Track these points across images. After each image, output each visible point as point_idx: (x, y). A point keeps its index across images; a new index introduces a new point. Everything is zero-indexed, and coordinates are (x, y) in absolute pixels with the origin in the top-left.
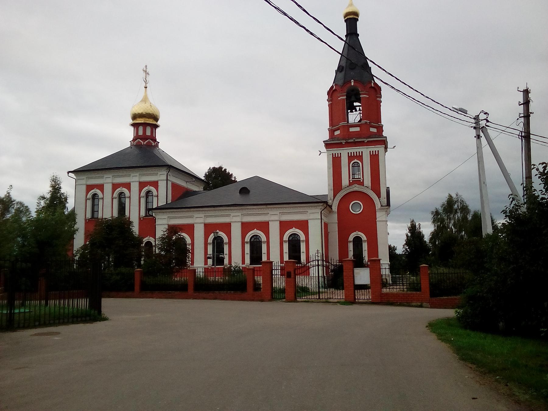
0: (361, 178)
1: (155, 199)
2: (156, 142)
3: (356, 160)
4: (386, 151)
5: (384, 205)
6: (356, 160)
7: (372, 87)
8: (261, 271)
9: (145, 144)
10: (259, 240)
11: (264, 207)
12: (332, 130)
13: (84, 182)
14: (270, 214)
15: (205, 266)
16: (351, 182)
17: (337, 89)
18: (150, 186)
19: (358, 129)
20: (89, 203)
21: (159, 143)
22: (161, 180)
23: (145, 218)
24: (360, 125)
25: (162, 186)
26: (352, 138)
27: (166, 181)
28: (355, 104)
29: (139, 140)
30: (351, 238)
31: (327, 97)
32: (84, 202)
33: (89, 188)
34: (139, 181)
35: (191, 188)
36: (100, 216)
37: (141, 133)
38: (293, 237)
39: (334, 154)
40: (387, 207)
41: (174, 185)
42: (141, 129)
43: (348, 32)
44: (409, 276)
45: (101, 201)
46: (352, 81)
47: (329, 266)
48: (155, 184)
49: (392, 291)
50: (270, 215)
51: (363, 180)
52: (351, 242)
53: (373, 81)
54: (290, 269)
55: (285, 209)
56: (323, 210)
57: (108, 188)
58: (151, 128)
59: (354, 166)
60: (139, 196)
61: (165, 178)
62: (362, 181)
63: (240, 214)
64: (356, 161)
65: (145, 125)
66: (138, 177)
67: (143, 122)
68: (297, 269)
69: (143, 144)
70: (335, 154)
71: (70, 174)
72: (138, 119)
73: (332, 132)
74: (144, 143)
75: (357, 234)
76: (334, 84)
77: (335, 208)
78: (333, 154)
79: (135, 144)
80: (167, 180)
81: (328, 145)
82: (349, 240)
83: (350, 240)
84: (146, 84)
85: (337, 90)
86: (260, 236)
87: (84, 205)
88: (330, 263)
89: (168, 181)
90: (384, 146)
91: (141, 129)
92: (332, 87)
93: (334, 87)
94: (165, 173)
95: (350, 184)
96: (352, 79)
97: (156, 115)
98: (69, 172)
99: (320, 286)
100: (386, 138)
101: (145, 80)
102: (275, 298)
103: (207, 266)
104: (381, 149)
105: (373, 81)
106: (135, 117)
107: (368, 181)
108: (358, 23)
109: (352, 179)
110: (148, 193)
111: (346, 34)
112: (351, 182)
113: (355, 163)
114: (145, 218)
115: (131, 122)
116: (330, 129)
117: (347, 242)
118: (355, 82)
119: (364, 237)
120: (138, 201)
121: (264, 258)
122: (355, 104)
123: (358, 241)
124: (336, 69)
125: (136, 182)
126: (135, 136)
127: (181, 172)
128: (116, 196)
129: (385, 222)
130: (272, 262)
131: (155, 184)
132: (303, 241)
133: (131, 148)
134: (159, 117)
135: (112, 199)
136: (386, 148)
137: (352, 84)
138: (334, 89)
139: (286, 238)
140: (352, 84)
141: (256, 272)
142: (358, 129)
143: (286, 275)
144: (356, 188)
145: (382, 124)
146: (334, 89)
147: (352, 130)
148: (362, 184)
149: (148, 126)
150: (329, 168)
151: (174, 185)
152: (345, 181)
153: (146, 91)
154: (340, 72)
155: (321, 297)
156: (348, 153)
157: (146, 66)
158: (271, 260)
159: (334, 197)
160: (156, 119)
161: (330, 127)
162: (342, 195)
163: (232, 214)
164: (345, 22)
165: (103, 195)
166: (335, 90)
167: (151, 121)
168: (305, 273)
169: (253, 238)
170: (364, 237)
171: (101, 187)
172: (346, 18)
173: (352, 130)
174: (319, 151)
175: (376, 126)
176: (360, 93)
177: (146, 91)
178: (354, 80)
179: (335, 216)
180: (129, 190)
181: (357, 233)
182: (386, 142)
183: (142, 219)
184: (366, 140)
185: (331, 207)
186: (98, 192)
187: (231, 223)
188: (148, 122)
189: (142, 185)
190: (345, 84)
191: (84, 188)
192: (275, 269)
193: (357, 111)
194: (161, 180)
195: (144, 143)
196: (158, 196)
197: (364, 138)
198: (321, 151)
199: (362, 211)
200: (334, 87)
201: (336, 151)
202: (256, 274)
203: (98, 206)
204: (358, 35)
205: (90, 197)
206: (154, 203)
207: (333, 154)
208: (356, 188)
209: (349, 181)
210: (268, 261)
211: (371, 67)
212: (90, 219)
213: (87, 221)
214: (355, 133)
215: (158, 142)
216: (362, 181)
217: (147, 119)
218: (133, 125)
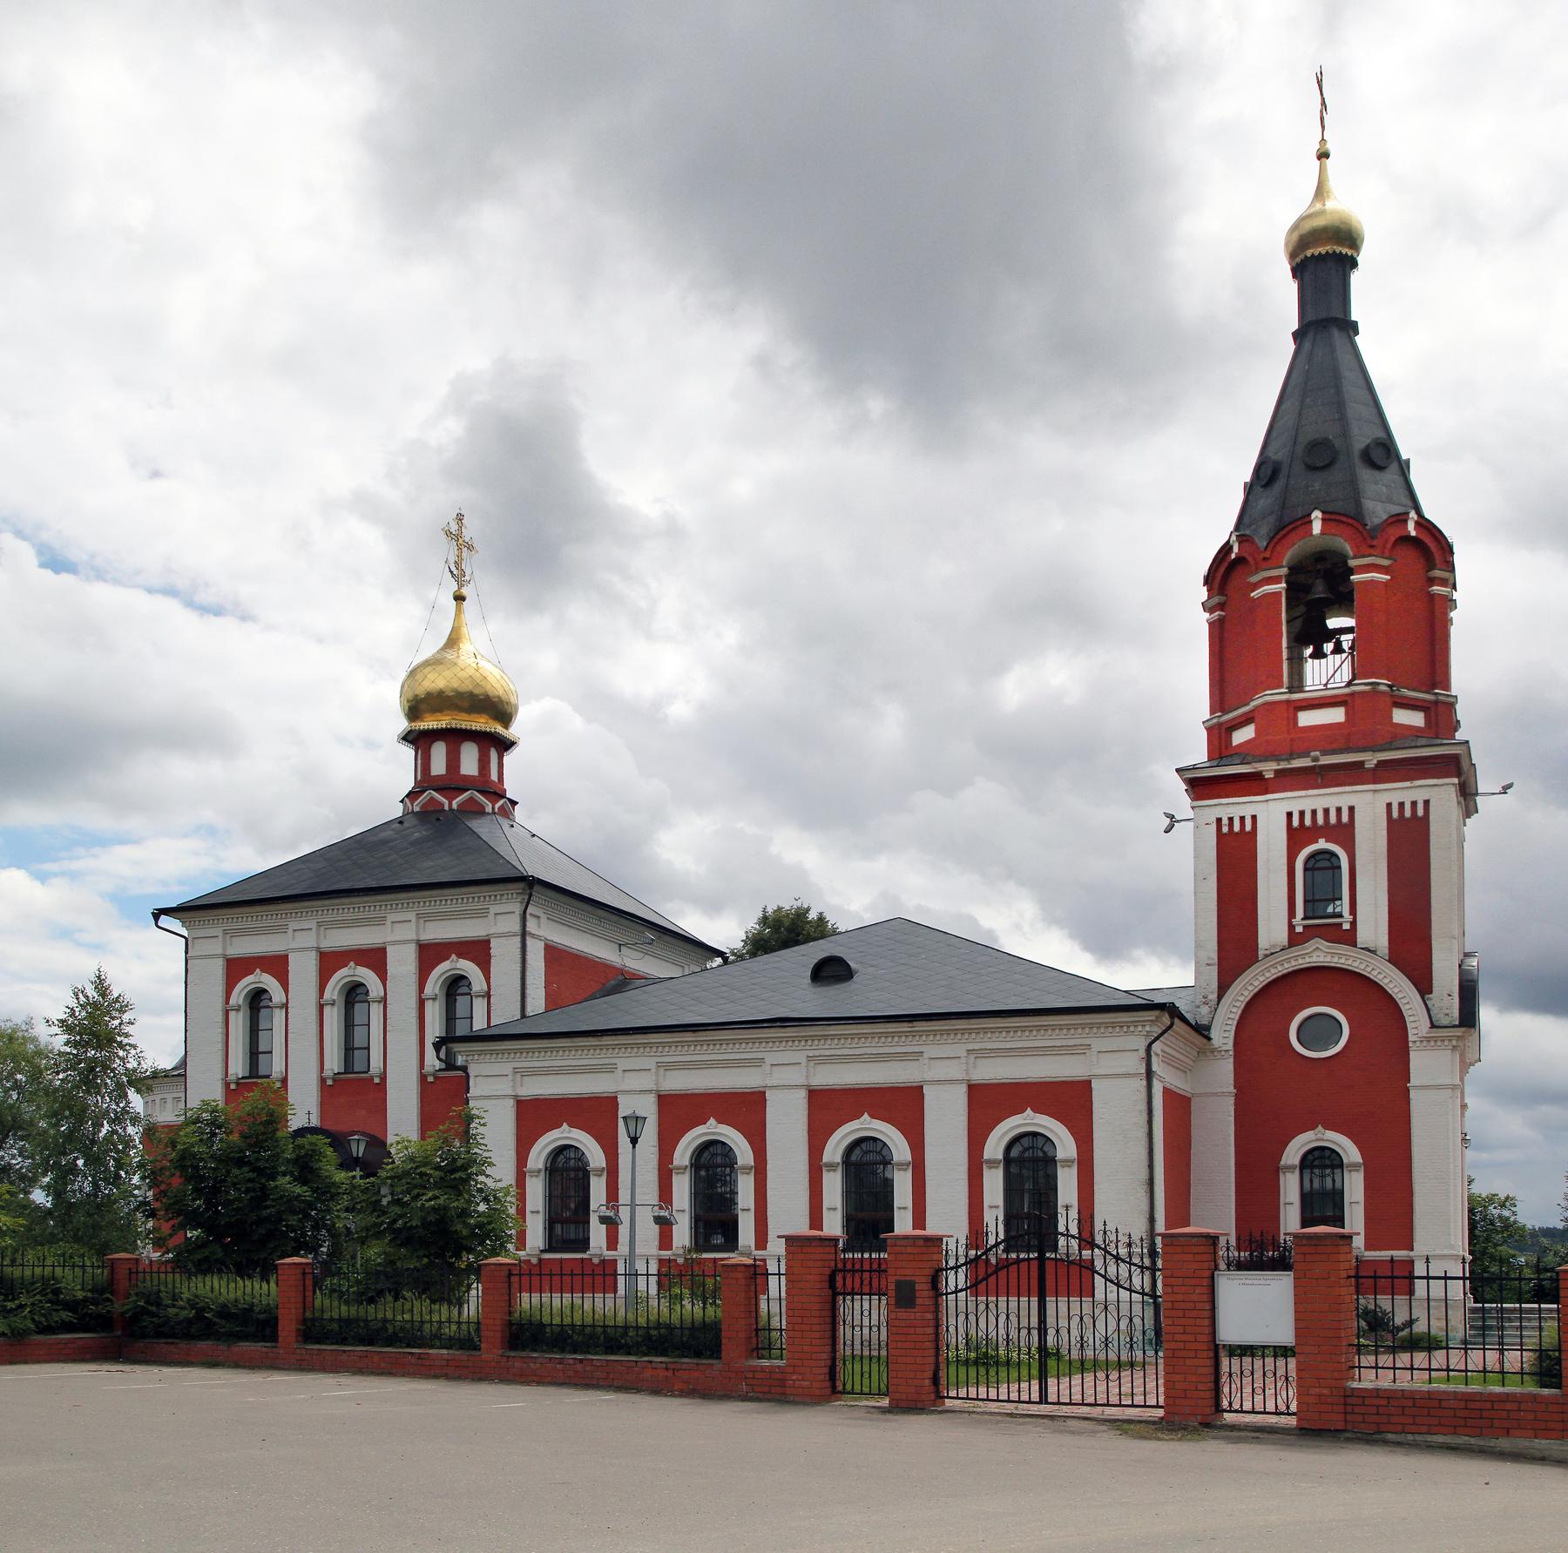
0: (1346, 913)
1: (479, 1006)
2: (501, 802)
4: (1469, 809)
5: (1445, 1022)
7: (1408, 538)
8: (1375, 1272)
9: (455, 806)
10: (883, 1157)
11: (905, 1027)
12: (1220, 725)
13: (216, 947)
14: (925, 1056)
15: (663, 1252)
16: (1299, 929)
17: (1246, 555)
18: (460, 956)
19: (1336, 715)
20: (239, 1022)
21: (514, 803)
22: (500, 936)
23: (441, 1074)
24: (1347, 698)
25: (504, 954)
26: (1305, 754)
27: (518, 939)
28: (1333, 623)
29: (432, 791)
30: (1293, 1152)
31: (1203, 593)
32: (220, 1018)
33: (236, 968)
34: (418, 941)
35: (585, 950)
36: (278, 1070)
37: (439, 766)
38: (1026, 1145)
39: (1225, 821)
40: (1459, 1032)
41: (554, 955)
42: (439, 752)
43: (1310, 317)
45: (279, 1015)
46: (1412, 518)
47: (1093, 1261)
48: (479, 951)
49: (1404, 1382)
50: (926, 1061)
51: (1354, 923)
52: (1290, 1168)
53: (1413, 515)
54: (908, 1272)
55: (989, 1035)
56: (1157, 1039)
57: (303, 969)
58: (480, 751)
59: (1313, 869)
60: (420, 996)
61: (517, 928)
62: (1346, 926)
63: (801, 1057)
64: (1322, 844)
65: (455, 737)
66: (414, 928)
67: (443, 724)
68: (844, 1270)
69: (446, 808)
70: (1231, 819)
71: (165, 921)
72: (428, 717)
73: (1219, 736)
74: (450, 804)
75: (1323, 1140)
76: (1234, 538)
77: (1223, 1035)
78: (1219, 820)
79: (417, 809)
80: (524, 934)
81: (1200, 786)
82: (1282, 1163)
83: (1289, 1162)
84: (460, 586)
85: (1250, 559)
86: (885, 1144)
87: (220, 1030)
88: (1099, 1247)
89: (528, 938)
90: (1456, 780)
91: (439, 752)
92: (1226, 549)
93: (1236, 549)
94: (517, 908)
95: (1295, 939)
96: (1315, 508)
97: (499, 697)
99: (1138, 1335)
100: (1464, 747)
101: (455, 572)
102: (844, 1392)
103: (669, 1253)
104: (1440, 795)
105: (1413, 515)
106: (414, 709)
107: (1373, 924)
108: (1356, 278)
109: (1304, 918)
110: (456, 984)
111: (1296, 327)
112: (1299, 929)
113: (1318, 858)
114: (441, 1074)
116: (1215, 721)
117: (1275, 1171)
118: (1329, 520)
119: (1350, 1151)
120: (414, 1014)
121: (903, 1224)
122: (1333, 623)
123: (1321, 1161)
124: (1248, 479)
126: (419, 778)
127: (589, 908)
128: (335, 997)
130: (936, 1241)
131: (479, 951)
132: (1067, 1162)
133: (401, 822)
134: (516, 708)
135: (321, 1008)
136: (1467, 795)
137: (1317, 527)
138: (1233, 556)
139: (994, 1147)
140: (1317, 527)
141: (514, 1279)
142: (1336, 715)
143: (892, 1293)
144: (1322, 954)
145: (1453, 693)
146: (1233, 556)
147: (1306, 719)
148: (1348, 938)
149: (467, 740)
150: (1199, 878)
151: (554, 955)
152: (1272, 925)
153: (459, 611)
154: (1262, 486)
155: (1052, 1397)
156: (1290, 815)
157: (460, 518)
158: (932, 1229)
159: (1223, 988)
160: (505, 716)
161: (1211, 713)
162: (1256, 983)
163: (770, 1058)
165: (287, 997)
166: (1240, 560)
167: (481, 723)
168: (992, 1279)
169: (857, 1151)
170: (1350, 1151)
171: (278, 965)
172: (1298, 260)
173: (1306, 719)
174: (1167, 815)
175: (1424, 701)
176: (1352, 563)
177: (459, 611)
178: (1323, 512)
179: (1223, 1073)
180: (382, 974)
181: (1320, 1136)
182: (1465, 765)
183: (430, 1079)
184: (1371, 759)
185: (1202, 1030)
186: (269, 982)
187: (765, 1092)
188: (464, 725)
189: (430, 954)
190: (1281, 534)
191: (217, 969)
192: (875, 1271)
193: (1344, 651)
194: (500, 936)
195: (450, 804)
196: (488, 995)
197: (1364, 750)
198: (1173, 817)
200: (1236, 549)
201: (1235, 808)
202: (515, 1286)
203: (367, 1051)
204: (1353, 328)
205: (241, 1002)
206: (474, 1019)
207: (1219, 820)
208: (1319, 953)
209: (1291, 927)
210: (919, 1232)
211: (1408, 462)
212: (243, 1078)
213: (233, 1086)
214: (1326, 737)
215: (509, 800)
216: (1346, 926)
217: (464, 716)
218: (410, 738)
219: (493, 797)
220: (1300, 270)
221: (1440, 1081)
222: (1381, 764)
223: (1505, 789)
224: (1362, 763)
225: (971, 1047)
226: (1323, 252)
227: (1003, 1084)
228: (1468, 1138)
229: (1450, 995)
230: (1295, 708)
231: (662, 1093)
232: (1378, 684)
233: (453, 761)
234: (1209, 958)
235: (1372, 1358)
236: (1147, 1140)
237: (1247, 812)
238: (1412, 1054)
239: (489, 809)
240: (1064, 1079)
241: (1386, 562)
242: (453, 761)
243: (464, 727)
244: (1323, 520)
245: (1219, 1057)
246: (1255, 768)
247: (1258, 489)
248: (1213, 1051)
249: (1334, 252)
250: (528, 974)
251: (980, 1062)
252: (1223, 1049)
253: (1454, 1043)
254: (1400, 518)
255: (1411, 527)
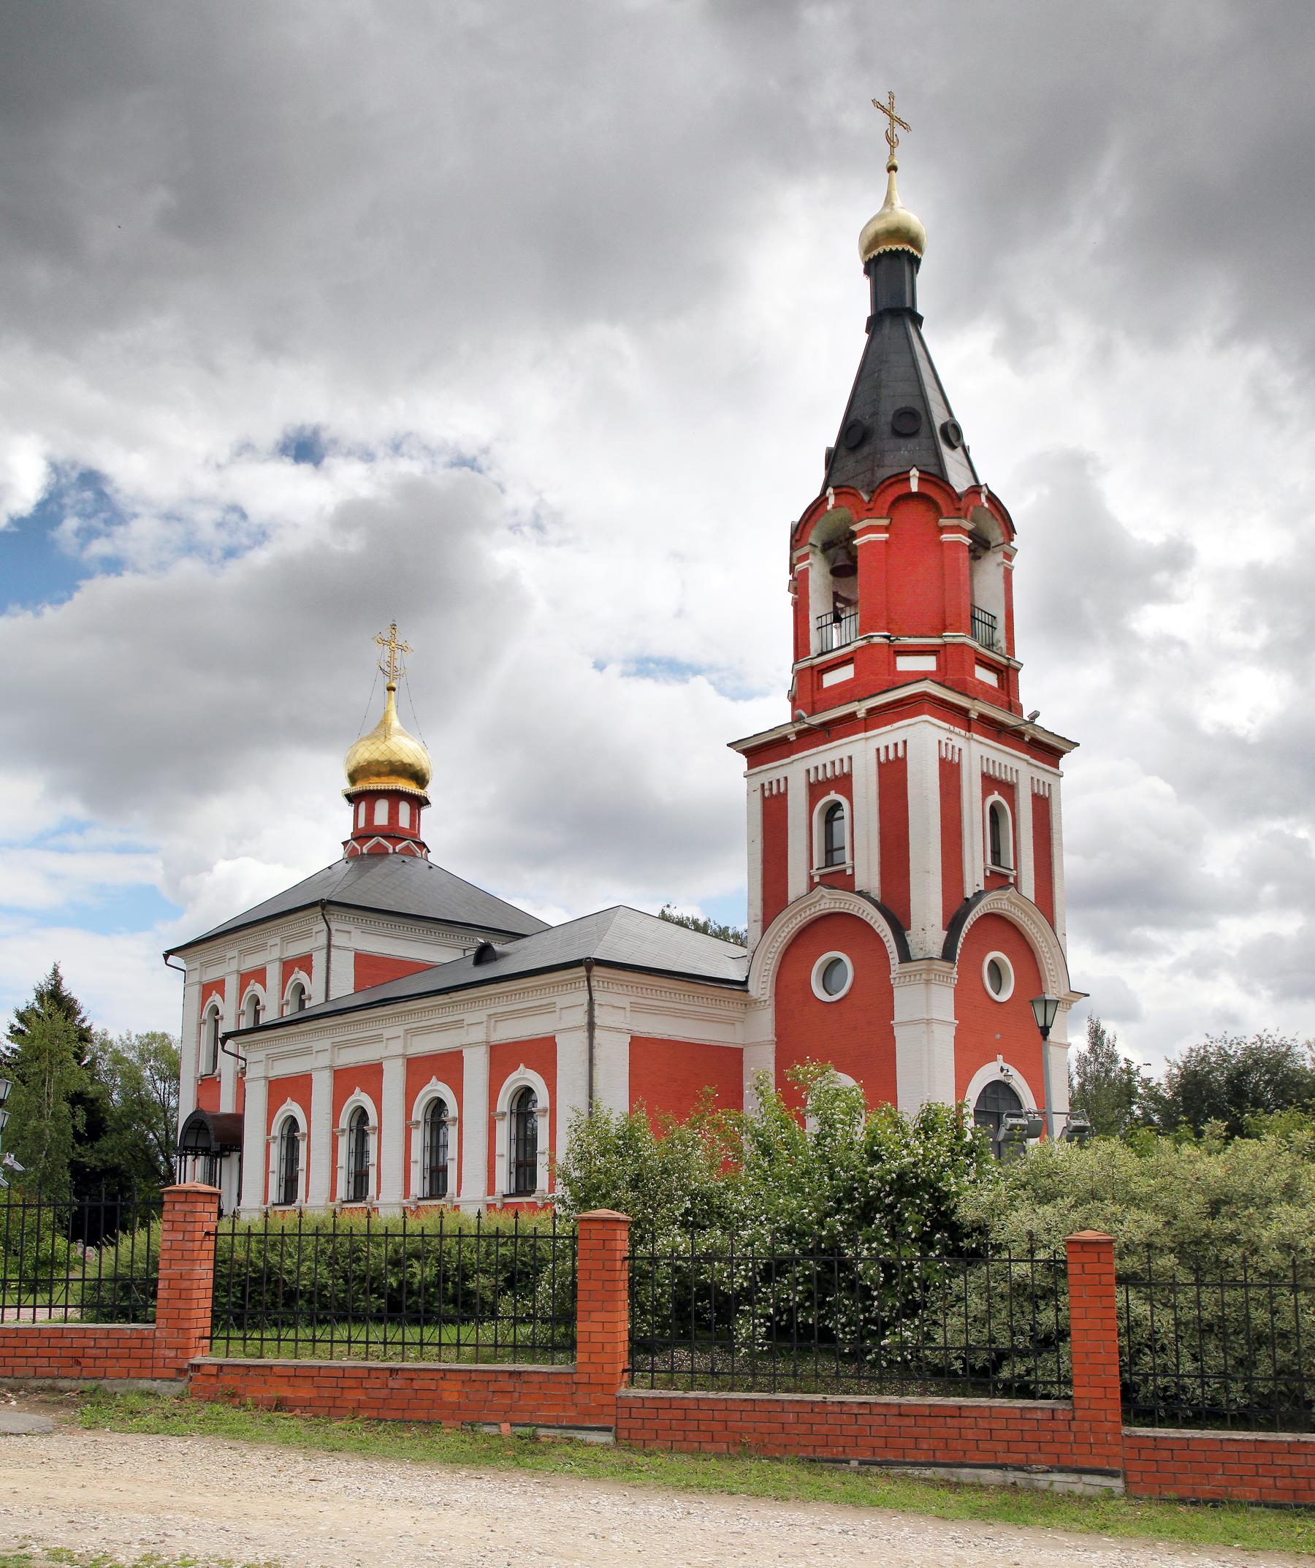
3: (832, 792)
6: (832, 792)
7: (911, 496)
9: (365, 851)
27: (325, 951)
39: (767, 786)
44: (678, 1156)
46: (914, 475)
48: (305, 962)
71: (172, 959)
74: (362, 849)
89: (332, 949)
93: (832, 501)
98: (167, 955)
106: (353, 778)
107: (867, 873)
115: (346, 786)
118: (842, 493)
125: (618, 1030)
129: (923, 1027)
142: (847, 673)
152: (797, 882)
156: (808, 771)
164: (867, 272)
172: (871, 255)
175: (999, 663)
178: (920, 471)
184: (861, 708)
191: (196, 991)
195: (394, 849)
199: (851, 989)
204: (918, 320)
208: (830, 901)
218: (352, 798)
219: (394, 841)
220: (871, 267)
221: (916, 1017)
222: (870, 711)
223: (394, 627)
224: (853, 715)
225: (492, 1011)
226: (894, 249)
227: (509, 1043)
228: (1009, 1073)
229: (923, 930)
230: (895, 652)
231: (336, 1068)
232: (872, 637)
233: (393, 814)
234: (756, 915)
235: (309, 1331)
236: (588, 1087)
237: (779, 774)
238: (895, 991)
239: (391, 851)
240: (542, 1036)
241: (885, 522)
242: (393, 814)
243: (372, 788)
244: (920, 479)
245: (762, 1008)
246: (780, 733)
247: (843, 452)
248: (755, 1001)
249: (903, 249)
250: (332, 978)
251: (500, 1025)
252: (762, 999)
253: (924, 976)
254: (901, 477)
255: (983, 499)
